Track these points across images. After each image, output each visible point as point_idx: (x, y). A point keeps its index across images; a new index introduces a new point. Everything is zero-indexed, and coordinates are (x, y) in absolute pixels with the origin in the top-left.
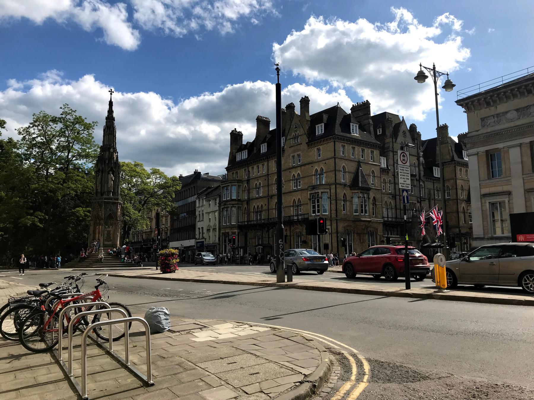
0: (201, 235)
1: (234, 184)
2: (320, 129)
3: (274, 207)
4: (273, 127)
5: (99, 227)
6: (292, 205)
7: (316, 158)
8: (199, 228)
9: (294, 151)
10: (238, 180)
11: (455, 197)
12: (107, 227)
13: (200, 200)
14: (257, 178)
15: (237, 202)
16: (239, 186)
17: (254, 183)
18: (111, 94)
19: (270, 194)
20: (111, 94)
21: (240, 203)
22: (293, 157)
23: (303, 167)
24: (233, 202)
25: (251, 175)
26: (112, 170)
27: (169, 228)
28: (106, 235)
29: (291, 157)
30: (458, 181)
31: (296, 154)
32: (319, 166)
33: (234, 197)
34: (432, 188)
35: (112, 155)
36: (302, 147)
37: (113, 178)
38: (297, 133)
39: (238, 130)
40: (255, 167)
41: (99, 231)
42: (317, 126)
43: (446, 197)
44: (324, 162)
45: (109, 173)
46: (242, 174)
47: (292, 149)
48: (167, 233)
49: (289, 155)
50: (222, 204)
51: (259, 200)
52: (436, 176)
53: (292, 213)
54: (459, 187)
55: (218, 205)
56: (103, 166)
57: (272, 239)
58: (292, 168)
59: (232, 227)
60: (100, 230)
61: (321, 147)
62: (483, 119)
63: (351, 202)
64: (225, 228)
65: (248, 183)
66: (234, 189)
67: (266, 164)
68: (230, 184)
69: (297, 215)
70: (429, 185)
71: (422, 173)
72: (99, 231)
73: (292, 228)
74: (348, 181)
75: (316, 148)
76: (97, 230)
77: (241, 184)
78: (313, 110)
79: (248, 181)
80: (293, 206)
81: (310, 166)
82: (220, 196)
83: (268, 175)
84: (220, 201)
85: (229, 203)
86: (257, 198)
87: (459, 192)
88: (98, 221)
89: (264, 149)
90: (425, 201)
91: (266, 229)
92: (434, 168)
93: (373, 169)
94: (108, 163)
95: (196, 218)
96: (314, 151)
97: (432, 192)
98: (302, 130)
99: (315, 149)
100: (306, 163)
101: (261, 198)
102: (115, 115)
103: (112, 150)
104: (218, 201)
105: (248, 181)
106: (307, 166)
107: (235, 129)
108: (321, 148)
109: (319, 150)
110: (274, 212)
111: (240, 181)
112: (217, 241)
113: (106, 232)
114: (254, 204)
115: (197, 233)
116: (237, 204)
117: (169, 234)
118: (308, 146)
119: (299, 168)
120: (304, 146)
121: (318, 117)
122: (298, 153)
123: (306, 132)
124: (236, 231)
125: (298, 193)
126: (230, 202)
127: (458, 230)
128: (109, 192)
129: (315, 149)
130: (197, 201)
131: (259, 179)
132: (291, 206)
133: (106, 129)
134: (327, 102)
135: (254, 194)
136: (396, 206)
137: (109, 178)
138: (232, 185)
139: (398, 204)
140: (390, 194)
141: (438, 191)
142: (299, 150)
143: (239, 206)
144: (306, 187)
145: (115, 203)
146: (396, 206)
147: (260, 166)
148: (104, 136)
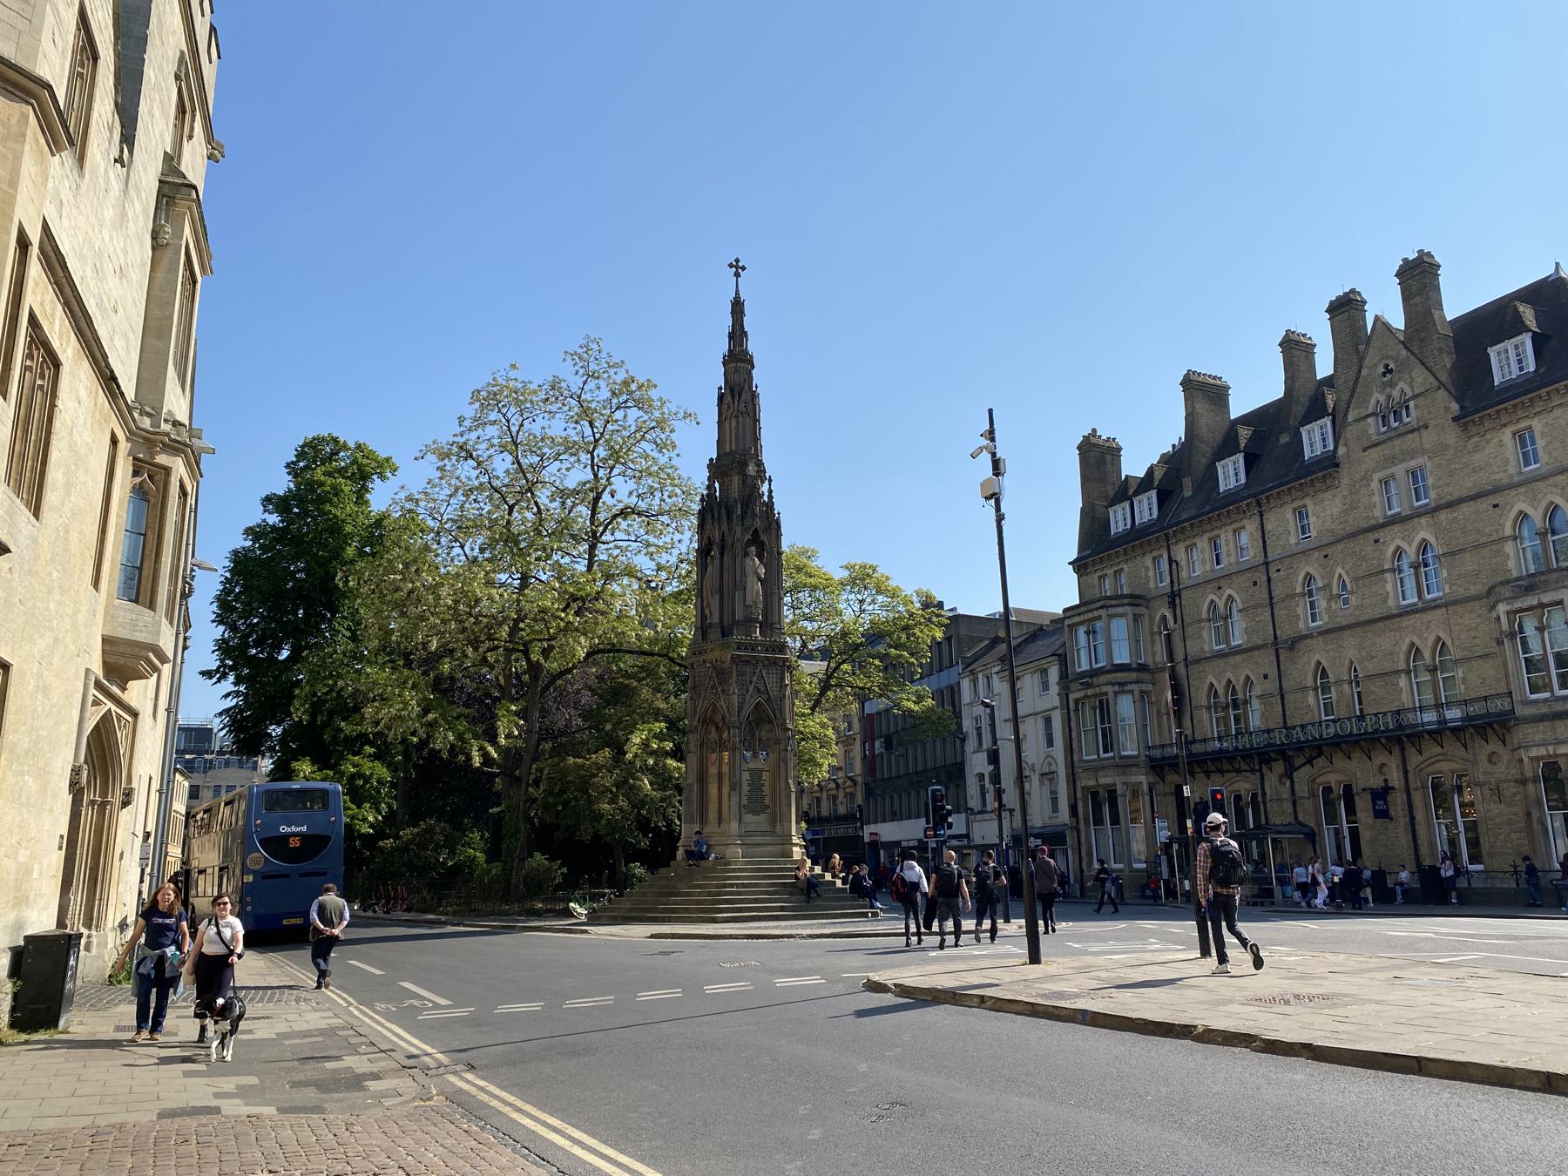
0: (990, 797)
1: (1120, 610)
2: (1511, 359)
3: (1310, 683)
4: (1324, 365)
5: (721, 760)
6: (1402, 666)
7: (1512, 471)
8: (981, 776)
10: (1131, 596)
12: (748, 754)
13: (975, 682)
14: (1216, 582)
15: (1134, 676)
16: (1136, 617)
17: (1200, 604)
18: (737, 275)
19: (1285, 632)
20: (737, 275)
21: (1145, 676)
22: (1385, 483)
23: (1443, 516)
24: (1120, 676)
25: (1184, 575)
26: (756, 540)
27: (859, 779)
28: (746, 788)
29: (1375, 485)
31: (1399, 470)
32: (1534, 502)
33: (1122, 656)
35: (756, 488)
36: (1428, 438)
37: (762, 571)
38: (1396, 393)
39: (1104, 434)
41: (720, 775)
42: (1492, 352)
45: (746, 554)
46: (1148, 572)
47: (1375, 454)
48: (852, 795)
49: (1366, 479)
50: (1074, 686)
51: (1231, 660)
53: (1405, 697)
55: (1054, 689)
56: (725, 526)
57: (1308, 804)
58: (1383, 526)
59: (1126, 765)
60: (725, 769)
61: (1537, 424)
64: (1095, 768)
65: (1172, 605)
66: (1120, 628)
67: (1251, 525)
68: (1102, 612)
69: (1438, 706)
72: (720, 775)
73: (1414, 759)
75: (1508, 431)
76: (713, 770)
77: (1143, 610)
78: (1459, 298)
79: (1173, 598)
80: (1408, 672)
81: (1484, 505)
82: (1063, 659)
83: (1267, 564)
84: (1064, 676)
85: (1103, 679)
86: (1221, 655)
88: (714, 735)
89: (1231, 473)
91: (1279, 767)
94: (743, 517)
95: (963, 740)
96: (1501, 444)
98: (1420, 374)
99: (1507, 435)
100: (1456, 495)
101: (1239, 651)
102: (753, 346)
103: (752, 469)
104: (1054, 674)
105: (1173, 598)
106: (1467, 508)
107: (1094, 430)
110: (1311, 699)
111: (1137, 599)
112: (1064, 815)
113: (746, 776)
114: (1210, 678)
115: (972, 789)
116: (1137, 682)
117: (859, 800)
118: (1465, 429)
119: (1423, 520)
120: (1452, 435)
121: (1495, 321)
122: (1413, 463)
123: (1444, 378)
124: (1143, 779)
125: (1428, 616)
126: (1110, 677)
128: (749, 621)
129: (1507, 435)
130: (966, 684)
131: (1223, 583)
132: (1397, 672)
133: (728, 398)
137: (749, 570)
138: (1111, 616)
142: (1411, 454)
143: (1144, 687)
145: (775, 662)
148: (719, 422)
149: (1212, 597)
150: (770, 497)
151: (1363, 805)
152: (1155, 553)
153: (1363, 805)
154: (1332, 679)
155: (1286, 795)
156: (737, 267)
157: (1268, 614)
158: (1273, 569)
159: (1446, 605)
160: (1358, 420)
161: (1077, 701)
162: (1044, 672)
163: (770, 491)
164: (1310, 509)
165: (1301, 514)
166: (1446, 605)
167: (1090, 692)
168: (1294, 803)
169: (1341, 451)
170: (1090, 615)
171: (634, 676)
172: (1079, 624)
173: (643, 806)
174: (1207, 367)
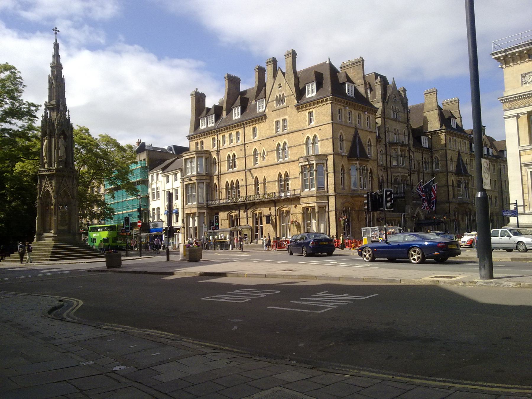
9: (279, 116)
11: (444, 169)
20: (56, 34)
30: (448, 151)
32: (311, 133)
34: (421, 159)
40: (227, 135)
43: (435, 169)
44: (318, 128)
52: (425, 146)
54: (449, 158)
55: (179, 180)
61: (257, 126)
62: (524, 76)
63: (349, 174)
70: (418, 156)
71: (412, 143)
74: (345, 151)
81: (300, 133)
83: (245, 144)
87: (449, 163)
90: (414, 173)
92: (422, 137)
93: (369, 137)
97: (421, 163)
99: (251, 127)
104: (179, 175)
106: (296, 133)
108: (314, 112)
109: (254, 129)
118: (298, 109)
119: (286, 136)
127: (447, 205)
131: (232, 149)
134: (219, 100)
135: (260, 162)
136: (387, 179)
139: (389, 177)
140: (382, 166)
141: (426, 162)
144: (296, 158)
146: (387, 179)
147: (227, 135)
149: (229, 153)
150: (69, 117)
151: (264, 219)
152: (213, 137)
153: (264, 219)
154: (240, 185)
155: (245, 217)
156: (56, 31)
157: (244, 160)
158: (246, 146)
159: (289, 162)
160: (271, 101)
161: (186, 185)
162: (176, 175)
163: (69, 115)
164: (257, 128)
165: (254, 129)
166: (289, 162)
167: (190, 182)
168: (247, 219)
169: (267, 111)
170: (191, 156)
171: (27, 130)
172: (189, 159)
173: (378, 220)
174: (233, 74)
